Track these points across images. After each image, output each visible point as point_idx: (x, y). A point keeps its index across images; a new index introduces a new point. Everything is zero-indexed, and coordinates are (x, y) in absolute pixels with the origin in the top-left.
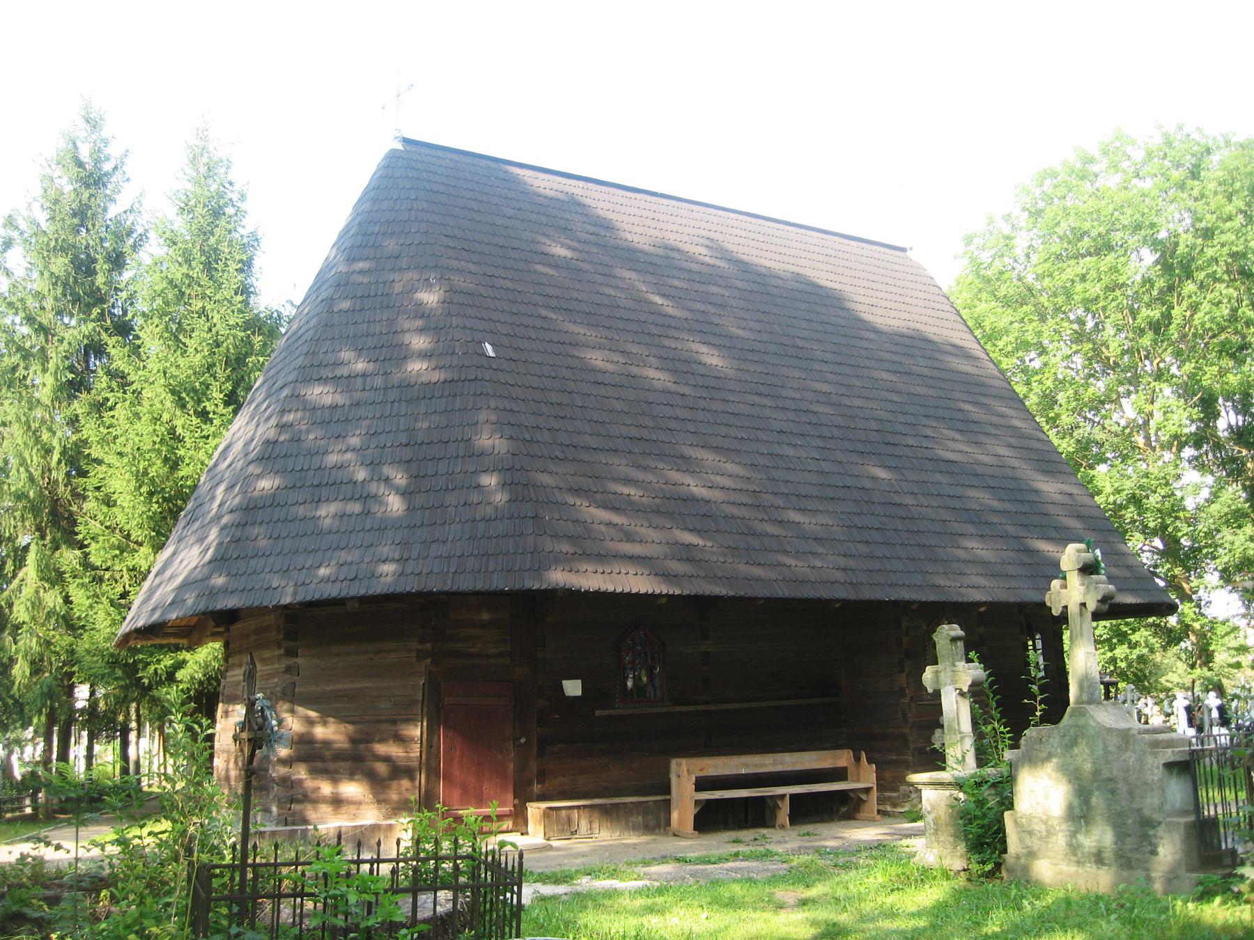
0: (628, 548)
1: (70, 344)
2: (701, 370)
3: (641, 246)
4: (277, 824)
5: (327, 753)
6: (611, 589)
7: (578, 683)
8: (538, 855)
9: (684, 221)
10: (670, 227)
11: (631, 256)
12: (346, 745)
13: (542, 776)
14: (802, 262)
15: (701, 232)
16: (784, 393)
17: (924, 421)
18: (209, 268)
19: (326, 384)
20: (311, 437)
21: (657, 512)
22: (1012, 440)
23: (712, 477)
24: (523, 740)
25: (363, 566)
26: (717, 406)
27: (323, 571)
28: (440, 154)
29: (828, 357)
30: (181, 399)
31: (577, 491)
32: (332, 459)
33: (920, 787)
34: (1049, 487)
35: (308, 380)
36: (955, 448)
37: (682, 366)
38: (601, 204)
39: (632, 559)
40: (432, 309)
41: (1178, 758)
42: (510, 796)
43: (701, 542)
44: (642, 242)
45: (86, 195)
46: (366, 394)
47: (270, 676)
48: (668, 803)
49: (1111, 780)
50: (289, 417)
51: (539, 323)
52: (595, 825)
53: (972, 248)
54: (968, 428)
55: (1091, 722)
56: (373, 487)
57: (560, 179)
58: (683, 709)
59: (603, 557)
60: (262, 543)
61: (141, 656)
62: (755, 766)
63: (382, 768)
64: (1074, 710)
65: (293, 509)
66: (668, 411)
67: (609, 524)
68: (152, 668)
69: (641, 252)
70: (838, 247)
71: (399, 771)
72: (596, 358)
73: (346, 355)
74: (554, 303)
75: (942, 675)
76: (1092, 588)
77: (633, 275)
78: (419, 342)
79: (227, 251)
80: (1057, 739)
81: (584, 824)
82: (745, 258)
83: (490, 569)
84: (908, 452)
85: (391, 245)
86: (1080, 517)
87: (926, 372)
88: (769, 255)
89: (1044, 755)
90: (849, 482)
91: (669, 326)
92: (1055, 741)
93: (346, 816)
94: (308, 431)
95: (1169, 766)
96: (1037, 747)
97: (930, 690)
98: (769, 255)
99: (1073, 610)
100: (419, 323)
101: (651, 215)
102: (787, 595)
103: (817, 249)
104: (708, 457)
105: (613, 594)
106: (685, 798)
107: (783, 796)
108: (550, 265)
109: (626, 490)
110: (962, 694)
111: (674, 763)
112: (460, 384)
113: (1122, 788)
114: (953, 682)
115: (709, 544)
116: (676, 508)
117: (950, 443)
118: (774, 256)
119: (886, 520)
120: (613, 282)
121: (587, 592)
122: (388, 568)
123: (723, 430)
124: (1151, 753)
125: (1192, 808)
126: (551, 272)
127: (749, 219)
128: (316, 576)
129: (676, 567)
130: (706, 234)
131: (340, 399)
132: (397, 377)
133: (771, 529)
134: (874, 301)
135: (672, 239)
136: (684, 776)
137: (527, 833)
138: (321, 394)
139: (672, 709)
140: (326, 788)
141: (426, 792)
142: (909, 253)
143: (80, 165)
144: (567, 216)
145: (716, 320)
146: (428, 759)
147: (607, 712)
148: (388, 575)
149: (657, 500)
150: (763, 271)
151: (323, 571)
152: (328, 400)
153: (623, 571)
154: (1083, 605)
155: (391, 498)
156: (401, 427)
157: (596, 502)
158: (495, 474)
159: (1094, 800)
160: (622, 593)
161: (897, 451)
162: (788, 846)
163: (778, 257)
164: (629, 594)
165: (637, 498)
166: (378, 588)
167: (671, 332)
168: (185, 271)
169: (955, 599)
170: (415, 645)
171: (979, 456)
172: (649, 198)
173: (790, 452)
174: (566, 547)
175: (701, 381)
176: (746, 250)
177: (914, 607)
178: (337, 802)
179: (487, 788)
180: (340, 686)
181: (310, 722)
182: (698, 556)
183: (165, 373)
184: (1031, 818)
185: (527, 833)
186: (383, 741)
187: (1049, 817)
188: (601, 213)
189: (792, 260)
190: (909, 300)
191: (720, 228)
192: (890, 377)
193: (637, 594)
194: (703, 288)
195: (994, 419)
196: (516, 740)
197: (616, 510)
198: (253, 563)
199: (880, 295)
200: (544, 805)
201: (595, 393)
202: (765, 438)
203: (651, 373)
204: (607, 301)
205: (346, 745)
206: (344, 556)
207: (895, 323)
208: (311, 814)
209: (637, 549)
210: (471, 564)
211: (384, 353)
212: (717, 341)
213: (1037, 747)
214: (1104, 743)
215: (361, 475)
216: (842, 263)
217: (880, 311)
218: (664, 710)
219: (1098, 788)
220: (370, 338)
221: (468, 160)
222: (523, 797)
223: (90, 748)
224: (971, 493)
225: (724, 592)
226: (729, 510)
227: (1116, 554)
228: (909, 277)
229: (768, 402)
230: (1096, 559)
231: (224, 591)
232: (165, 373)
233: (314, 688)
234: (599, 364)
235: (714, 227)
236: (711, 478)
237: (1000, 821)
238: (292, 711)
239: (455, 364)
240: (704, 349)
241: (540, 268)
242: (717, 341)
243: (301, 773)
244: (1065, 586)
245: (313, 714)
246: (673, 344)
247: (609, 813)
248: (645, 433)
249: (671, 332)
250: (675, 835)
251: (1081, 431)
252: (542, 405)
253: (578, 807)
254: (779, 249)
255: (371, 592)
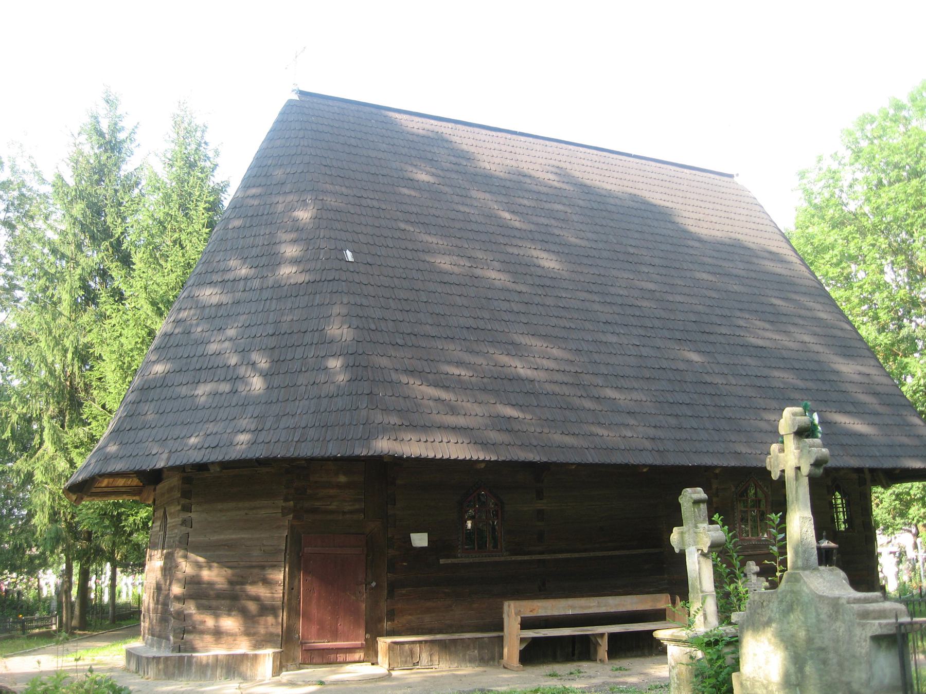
0: (451, 420)
1: (83, 269)
2: (539, 272)
3: (497, 173)
4: (173, 651)
5: (212, 593)
6: (431, 455)
7: (425, 536)
8: (369, 685)
9: (538, 154)
10: (524, 158)
11: (486, 180)
12: (225, 586)
13: (391, 615)
14: (640, 186)
15: (552, 162)
16: (613, 290)
17: (738, 314)
18: (183, 207)
19: (215, 287)
20: (199, 329)
21: (484, 390)
22: (818, 330)
23: (539, 360)
24: (374, 584)
25: (226, 436)
26: (549, 301)
27: (193, 440)
28: (330, 103)
29: (657, 261)
30: (159, 309)
31: (411, 372)
32: (213, 347)
33: (665, 643)
34: (848, 368)
35: (201, 284)
36: (763, 335)
37: (520, 268)
38: (464, 140)
39: (455, 429)
40: (305, 224)
41: (885, 631)
42: (362, 632)
43: (521, 416)
44: (498, 169)
45: (104, 158)
46: (246, 294)
47: (175, 527)
48: (501, 639)
49: (822, 649)
50: (183, 315)
51: (398, 234)
52: (436, 658)
53: (805, 181)
54: (776, 319)
55: (805, 589)
56: (242, 371)
57: (432, 122)
58: (519, 558)
59: (426, 428)
60: (150, 417)
61: (123, 510)
62: (581, 607)
63: (252, 607)
64: (791, 575)
65: (178, 389)
66: (505, 306)
67: (438, 400)
68: (131, 519)
69: (497, 178)
70: (673, 173)
71: (266, 609)
72: (444, 263)
73: (233, 263)
74: (413, 218)
75: (686, 535)
76: (805, 451)
77: (488, 196)
78: (291, 251)
79: (198, 194)
80: (776, 604)
81: (425, 657)
82: (588, 182)
83: (328, 439)
84: (722, 339)
85: (279, 173)
86: (875, 394)
87: (742, 273)
88: (611, 180)
89: (765, 619)
90: (665, 364)
91: (514, 237)
92: (774, 605)
93: (224, 646)
94: (197, 325)
95: (877, 639)
96: (759, 611)
97: (677, 551)
98: (611, 180)
99: (790, 474)
100: (293, 236)
101: (509, 149)
102: (597, 461)
103: (654, 176)
104: (537, 344)
105: (433, 460)
106: (514, 637)
107: (602, 635)
108: (414, 189)
109: (456, 371)
110: (704, 555)
111: (506, 604)
112: (321, 284)
113: (833, 659)
114: (696, 543)
115: (529, 417)
116: (502, 385)
117: (761, 332)
118: (614, 181)
119: (695, 396)
120: (468, 201)
121: (409, 459)
122: (243, 438)
123: (554, 321)
124: (859, 624)
125: (900, 683)
126: (413, 193)
127: (595, 152)
128: (186, 445)
129: (494, 436)
130: (556, 163)
131: (225, 299)
132: (270, 282)
133: (588, 404)
134: (701, 216)
135: (526, 167)
136: (513, 613)
137: (377, 663)
138: (209, 295)
139: (509, 558)
140: (210, 622)
141: (288, 627)
142: (736, 179)
143: (101, 134)
144: (435, 150)
145: (557, 232)
146: (289, 600)
147: (449, 561)
148: (242, 444)
149: (485, 380)
150: (604, 193)
151: (193, 440)
152: (215, 300)
153: (445, 440)
154: (798, 468)
155: (255, 378)
156: (270, 321)
157: (427, 381)
158: (340, 358)
159: (808, 669)
160: (441, 459)
161: (712, 338)
162: (594, 681)
163: (618, 182)
164: (448, 460)
165: (467, 378)
166: (233, 454)
167: (515, 242)
168: (166, 210)
169: (754, 464)
170: (281, 503)
171: (786, 343)
172: (509, 136)
173: (613, 339)
174: (394, 419)
175: (538, 281)
176: (591, 176)
177: (483, 466)
178: (218, 634)
179: (342, 626)
180: (222, 537)
181: (199, 566)
182: (516, 427)
183: (146, 289)
184: (754, 681)
185: (377, 663)
186: (253, 583)
187: (769, 682)
188: (464, 147)
189: (630, 184)
190: (732, 216)
191: (569, 159)
192: (710, 278)
193: (456, 460)
194: (548, 206)
195: (803, 312)
196: (368, 584)
197: (446, 388)
198: (141, 433)
199: (707, 212)
200: (389, 640)
201: (439, 290)
202: (591, 328)
203: (493, 274)
204: (461, 217)
205: (225, 586)
206: (211, 428)
207: (719, 234)
208: (198, 642)
209: (461, 421)
210: (312, 433)
211: (264, 260)
212: (554, 248)
213: (759, 611)
214: (817, 611)
215: (233, 360)
216: (675, 186)
217: (705, 225)
218: (503, 559)
219: (812, 657)
220: (254, 249)
221: (353, 107)
222: (374, 631)
223: (113, 578)
224: (776, 373)
225: (537, 459)
226: (549, 388)
227: (908, 425)
228: (735, 198)
229: (596, 298)
230: (812, 423)
231: (116, 457)
232: (146, 289)
233: (202, 538)
234: (447, 267)
235: (564, 158)
236: (536, 361)
237: (729, 681)
238: (185, 557)
239: (318, 267)
240: (544, 255)
241: (406, 191)
242: (554, 248)
243: (191, 608)
244: (782, 450)
245: (201, 559)
246: (516, 251)
247: (446, 648)
248: (481, 324)
249: (515, 242)
250: (505, 667)
251: (906, 329)
252: (391, 300)
253: (420, 642)
254: (620, 176)
255: (227, 458)
